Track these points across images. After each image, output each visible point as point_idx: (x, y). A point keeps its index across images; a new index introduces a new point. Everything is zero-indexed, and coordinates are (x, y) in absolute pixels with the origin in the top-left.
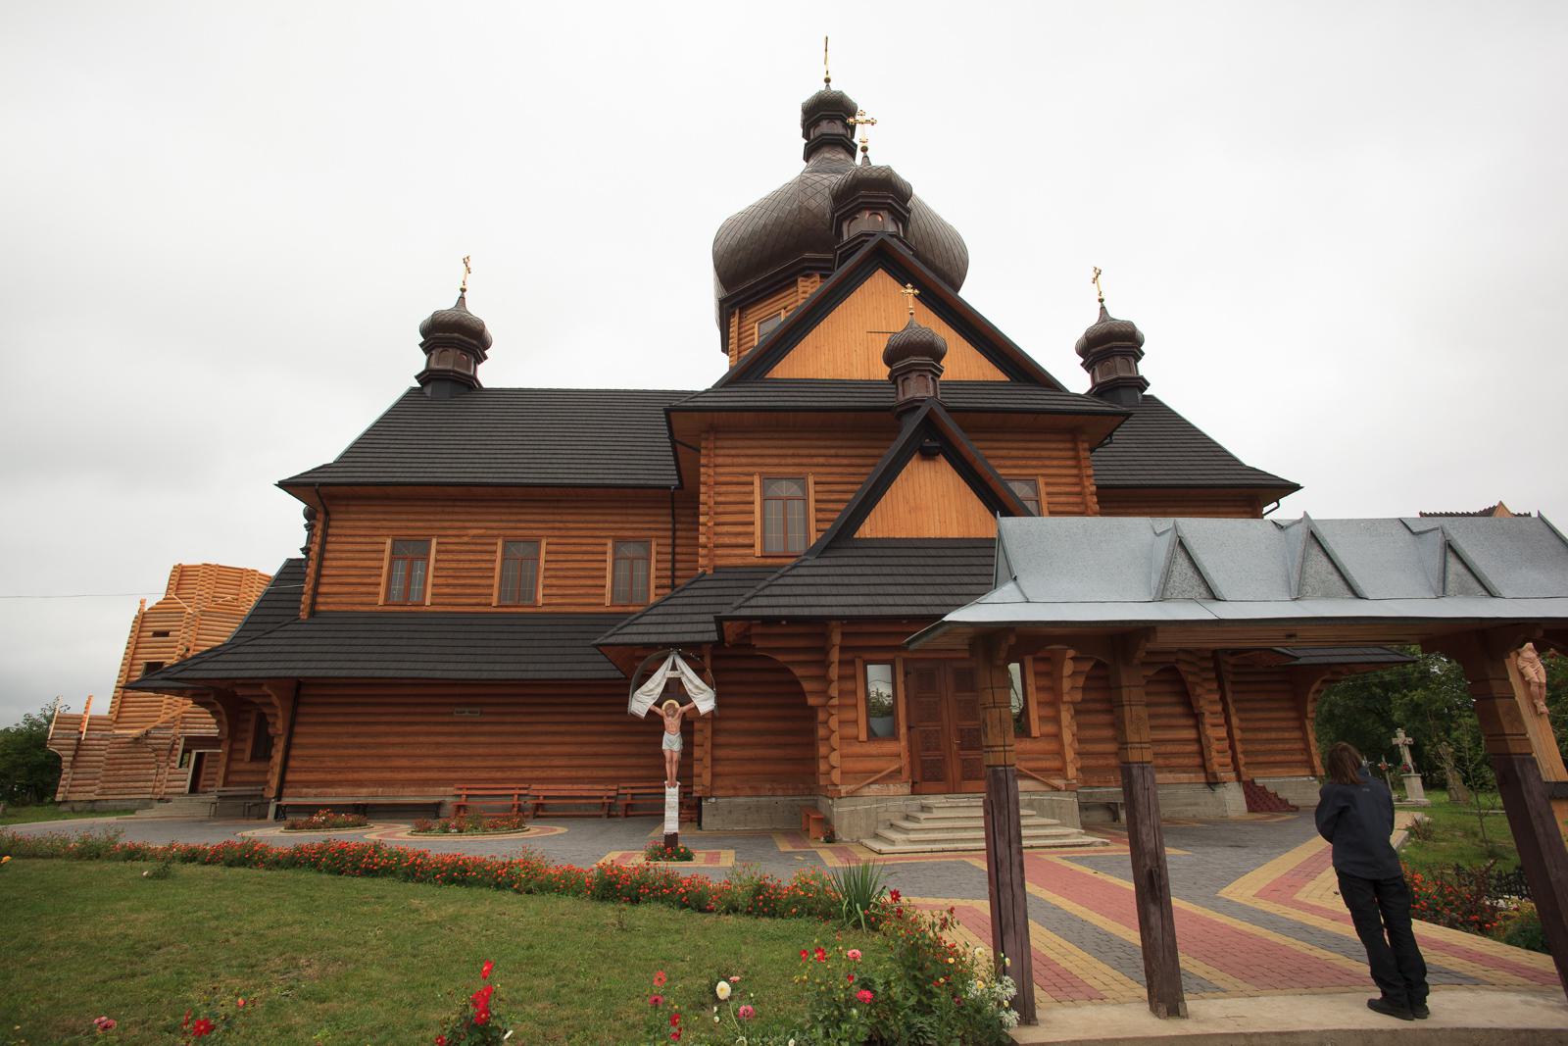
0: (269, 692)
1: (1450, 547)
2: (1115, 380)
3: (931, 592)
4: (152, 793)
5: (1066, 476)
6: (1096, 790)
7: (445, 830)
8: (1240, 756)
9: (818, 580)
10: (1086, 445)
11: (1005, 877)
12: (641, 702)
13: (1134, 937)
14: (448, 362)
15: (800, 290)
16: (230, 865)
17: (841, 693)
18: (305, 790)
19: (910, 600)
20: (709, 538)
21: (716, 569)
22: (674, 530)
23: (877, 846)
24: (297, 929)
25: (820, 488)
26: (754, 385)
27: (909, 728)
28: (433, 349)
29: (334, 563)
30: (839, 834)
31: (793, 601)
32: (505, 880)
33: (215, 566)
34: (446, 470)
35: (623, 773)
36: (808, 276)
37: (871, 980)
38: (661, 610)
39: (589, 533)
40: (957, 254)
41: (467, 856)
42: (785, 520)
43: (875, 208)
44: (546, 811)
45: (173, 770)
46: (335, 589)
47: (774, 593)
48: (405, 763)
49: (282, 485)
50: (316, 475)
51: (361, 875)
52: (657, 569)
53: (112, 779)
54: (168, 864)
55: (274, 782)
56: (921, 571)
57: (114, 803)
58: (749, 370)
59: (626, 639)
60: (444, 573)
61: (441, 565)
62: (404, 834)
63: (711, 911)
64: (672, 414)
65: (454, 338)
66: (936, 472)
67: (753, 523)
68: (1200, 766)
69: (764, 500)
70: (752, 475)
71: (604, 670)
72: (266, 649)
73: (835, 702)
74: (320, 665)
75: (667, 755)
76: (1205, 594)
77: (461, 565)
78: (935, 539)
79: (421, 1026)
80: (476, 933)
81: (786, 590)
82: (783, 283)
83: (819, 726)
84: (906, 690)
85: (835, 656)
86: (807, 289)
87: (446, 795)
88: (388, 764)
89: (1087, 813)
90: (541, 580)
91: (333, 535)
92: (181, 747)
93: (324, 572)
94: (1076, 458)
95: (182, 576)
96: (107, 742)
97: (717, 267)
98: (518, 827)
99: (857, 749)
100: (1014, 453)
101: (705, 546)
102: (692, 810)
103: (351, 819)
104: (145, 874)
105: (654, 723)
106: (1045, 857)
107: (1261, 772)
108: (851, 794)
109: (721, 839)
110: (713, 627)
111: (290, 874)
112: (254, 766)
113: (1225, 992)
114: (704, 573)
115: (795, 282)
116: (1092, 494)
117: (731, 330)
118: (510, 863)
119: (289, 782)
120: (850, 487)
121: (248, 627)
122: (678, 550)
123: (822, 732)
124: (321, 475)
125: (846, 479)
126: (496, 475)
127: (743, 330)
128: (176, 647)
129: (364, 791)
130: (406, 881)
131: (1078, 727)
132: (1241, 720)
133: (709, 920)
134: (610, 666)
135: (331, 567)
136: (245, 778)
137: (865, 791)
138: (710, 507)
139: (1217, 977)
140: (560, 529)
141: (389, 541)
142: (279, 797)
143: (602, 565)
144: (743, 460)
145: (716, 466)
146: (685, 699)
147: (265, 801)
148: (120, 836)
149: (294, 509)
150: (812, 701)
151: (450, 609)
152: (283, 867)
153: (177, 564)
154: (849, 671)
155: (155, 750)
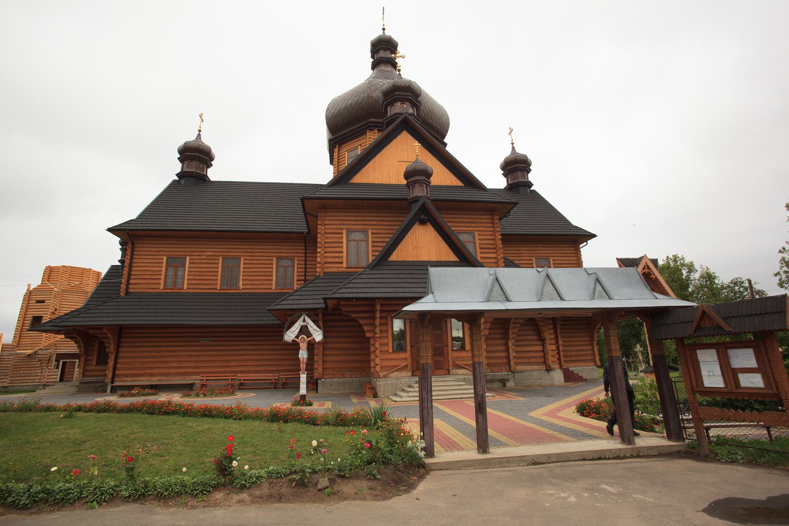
0: (107, 332)
1: (598, 280)
2: (517, 182)
3: (421, 286)
4: (39, 382)
5: (488, 231)
6: (496, 373)
7: (198, 395)
8: (562, 358)
9: (371, 281)
10: (497, 217)
11: (425, 405)
12: (290, 335)
13: (474, 424)
14: (193, 168)
15: (368, 137)
16: (99, 412)
17: (381, 331)
18: (125, 378)
19: (411, 290)
20: (321, 259)
21: (325, 273)
22: (306, 253)
23: (394, 398)
24: (142, 434)
25: (374, 236)
26: (344, 186)
27: (411, 347)
28: (185, 160)
29: (138, 269)
30: (379, 394)
31: (359, 290)
32: (229, 415)
33: (68, 267)
34: (193, 223)
35: (282, 368)
36: (372, 130)
37: (371, 441)
38: (299, 293)
39: (265, 254)
40: (444, 120)
41: (211, 405)
42: (358, 250)
43: (403, 101)
44: (245, 386)
45: (50, 370)
46: (138, 281)
47: (350, 287)
48: (176, 365)
49: (110, 230)
50: (127, 225)
51: (163, 415)
52: (297, 272)
53: (16, 375)
54: (71, 412)
55: (110, 375)
56: (418, 276)
57: (18, 387)
58: (342, 178)
59: (282, 307)
60: (193, 274)
61: (192, 269)
62: (178, 398)
63: (318, 425)
64: (304, 200)
65: (195, 156)
66: (426, 230)
67: (342, 252)
68: (543, 362)
69: (348, 241)
70: (342, 229)
71: (272, 320)
72: (105, 311)
73: (378, 335)
74: (132, 318)
75: (301, 360)
76: (505, 299)
77: (202, 270)
78: (425, 261)
79: (203, 463)
80: (219, 434)
81: (356, 285)
82: (359, 133)
83: (371, 346)
84: (411, 333)
85: (378, 315)
86: (372, 137)
87: (196, 379)
88: (167, 366)
89: (492, 384)
90: (241, 277)
91: (136, 255)
92: (54, 359)
93: (132, 273)
94: (493, 223)
95: (50, 273)
96: (13, 357)
97: (328, 123)
98: (232, 393)
99: (388, 356)
100: (465, 220)
101: (319, 263)
102: (313, 384)
103: (150, 392)
104: (61, 416)
105: (295, 346)
106: (467, 402)
107: (573, 364)
108: (385, 376)
109: (326, 397)
110: (322, 301)
111: (129, 415)
112: (98, 367)
113: (508, 445)
114: (319, 276)
115: (365, 133)
116: (499, 240)
117: (334, 155)
118: (231, 407)
119: (117, 375)
120: (388, 235)
121: (93, 299)
122: (308, 263)
123: (372, 349)
124: (130, 225)
125: (386, 232)
126: (218, 226)
127: (340, 155)
128: (49, 308)
129: (155, 378)
130: (184, 416)
131: (486, 345)
132: (563, 342)
133: (317, 428)
134: (275, 318)
135: (136, 270)
136: (93, 373)
137: (391, 375)
138: (322, 245)
139: (503, 439)
140: (250, 252)
141: (165, 258)
142: (112, 382)
143: (271, 270)
144: (338, 222)
145: (325, 225)
146: (309, 335)
147: (105, 384)
148: (41, 401)
149: (115, 241)
150: (368, 335)
151: (196, 291)
152: (125, 412)
153: (48, 266)
154: (384, 321)
155: (40, 360)
